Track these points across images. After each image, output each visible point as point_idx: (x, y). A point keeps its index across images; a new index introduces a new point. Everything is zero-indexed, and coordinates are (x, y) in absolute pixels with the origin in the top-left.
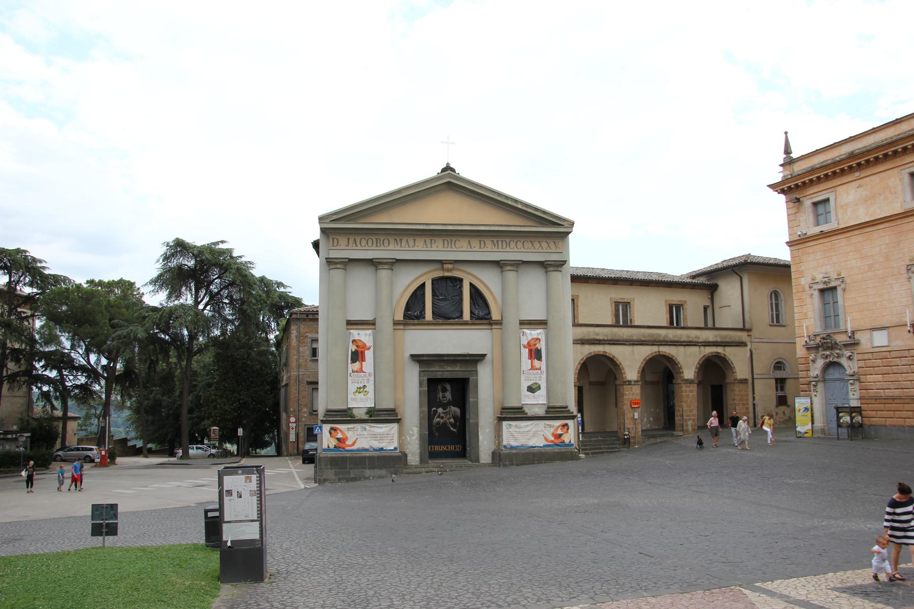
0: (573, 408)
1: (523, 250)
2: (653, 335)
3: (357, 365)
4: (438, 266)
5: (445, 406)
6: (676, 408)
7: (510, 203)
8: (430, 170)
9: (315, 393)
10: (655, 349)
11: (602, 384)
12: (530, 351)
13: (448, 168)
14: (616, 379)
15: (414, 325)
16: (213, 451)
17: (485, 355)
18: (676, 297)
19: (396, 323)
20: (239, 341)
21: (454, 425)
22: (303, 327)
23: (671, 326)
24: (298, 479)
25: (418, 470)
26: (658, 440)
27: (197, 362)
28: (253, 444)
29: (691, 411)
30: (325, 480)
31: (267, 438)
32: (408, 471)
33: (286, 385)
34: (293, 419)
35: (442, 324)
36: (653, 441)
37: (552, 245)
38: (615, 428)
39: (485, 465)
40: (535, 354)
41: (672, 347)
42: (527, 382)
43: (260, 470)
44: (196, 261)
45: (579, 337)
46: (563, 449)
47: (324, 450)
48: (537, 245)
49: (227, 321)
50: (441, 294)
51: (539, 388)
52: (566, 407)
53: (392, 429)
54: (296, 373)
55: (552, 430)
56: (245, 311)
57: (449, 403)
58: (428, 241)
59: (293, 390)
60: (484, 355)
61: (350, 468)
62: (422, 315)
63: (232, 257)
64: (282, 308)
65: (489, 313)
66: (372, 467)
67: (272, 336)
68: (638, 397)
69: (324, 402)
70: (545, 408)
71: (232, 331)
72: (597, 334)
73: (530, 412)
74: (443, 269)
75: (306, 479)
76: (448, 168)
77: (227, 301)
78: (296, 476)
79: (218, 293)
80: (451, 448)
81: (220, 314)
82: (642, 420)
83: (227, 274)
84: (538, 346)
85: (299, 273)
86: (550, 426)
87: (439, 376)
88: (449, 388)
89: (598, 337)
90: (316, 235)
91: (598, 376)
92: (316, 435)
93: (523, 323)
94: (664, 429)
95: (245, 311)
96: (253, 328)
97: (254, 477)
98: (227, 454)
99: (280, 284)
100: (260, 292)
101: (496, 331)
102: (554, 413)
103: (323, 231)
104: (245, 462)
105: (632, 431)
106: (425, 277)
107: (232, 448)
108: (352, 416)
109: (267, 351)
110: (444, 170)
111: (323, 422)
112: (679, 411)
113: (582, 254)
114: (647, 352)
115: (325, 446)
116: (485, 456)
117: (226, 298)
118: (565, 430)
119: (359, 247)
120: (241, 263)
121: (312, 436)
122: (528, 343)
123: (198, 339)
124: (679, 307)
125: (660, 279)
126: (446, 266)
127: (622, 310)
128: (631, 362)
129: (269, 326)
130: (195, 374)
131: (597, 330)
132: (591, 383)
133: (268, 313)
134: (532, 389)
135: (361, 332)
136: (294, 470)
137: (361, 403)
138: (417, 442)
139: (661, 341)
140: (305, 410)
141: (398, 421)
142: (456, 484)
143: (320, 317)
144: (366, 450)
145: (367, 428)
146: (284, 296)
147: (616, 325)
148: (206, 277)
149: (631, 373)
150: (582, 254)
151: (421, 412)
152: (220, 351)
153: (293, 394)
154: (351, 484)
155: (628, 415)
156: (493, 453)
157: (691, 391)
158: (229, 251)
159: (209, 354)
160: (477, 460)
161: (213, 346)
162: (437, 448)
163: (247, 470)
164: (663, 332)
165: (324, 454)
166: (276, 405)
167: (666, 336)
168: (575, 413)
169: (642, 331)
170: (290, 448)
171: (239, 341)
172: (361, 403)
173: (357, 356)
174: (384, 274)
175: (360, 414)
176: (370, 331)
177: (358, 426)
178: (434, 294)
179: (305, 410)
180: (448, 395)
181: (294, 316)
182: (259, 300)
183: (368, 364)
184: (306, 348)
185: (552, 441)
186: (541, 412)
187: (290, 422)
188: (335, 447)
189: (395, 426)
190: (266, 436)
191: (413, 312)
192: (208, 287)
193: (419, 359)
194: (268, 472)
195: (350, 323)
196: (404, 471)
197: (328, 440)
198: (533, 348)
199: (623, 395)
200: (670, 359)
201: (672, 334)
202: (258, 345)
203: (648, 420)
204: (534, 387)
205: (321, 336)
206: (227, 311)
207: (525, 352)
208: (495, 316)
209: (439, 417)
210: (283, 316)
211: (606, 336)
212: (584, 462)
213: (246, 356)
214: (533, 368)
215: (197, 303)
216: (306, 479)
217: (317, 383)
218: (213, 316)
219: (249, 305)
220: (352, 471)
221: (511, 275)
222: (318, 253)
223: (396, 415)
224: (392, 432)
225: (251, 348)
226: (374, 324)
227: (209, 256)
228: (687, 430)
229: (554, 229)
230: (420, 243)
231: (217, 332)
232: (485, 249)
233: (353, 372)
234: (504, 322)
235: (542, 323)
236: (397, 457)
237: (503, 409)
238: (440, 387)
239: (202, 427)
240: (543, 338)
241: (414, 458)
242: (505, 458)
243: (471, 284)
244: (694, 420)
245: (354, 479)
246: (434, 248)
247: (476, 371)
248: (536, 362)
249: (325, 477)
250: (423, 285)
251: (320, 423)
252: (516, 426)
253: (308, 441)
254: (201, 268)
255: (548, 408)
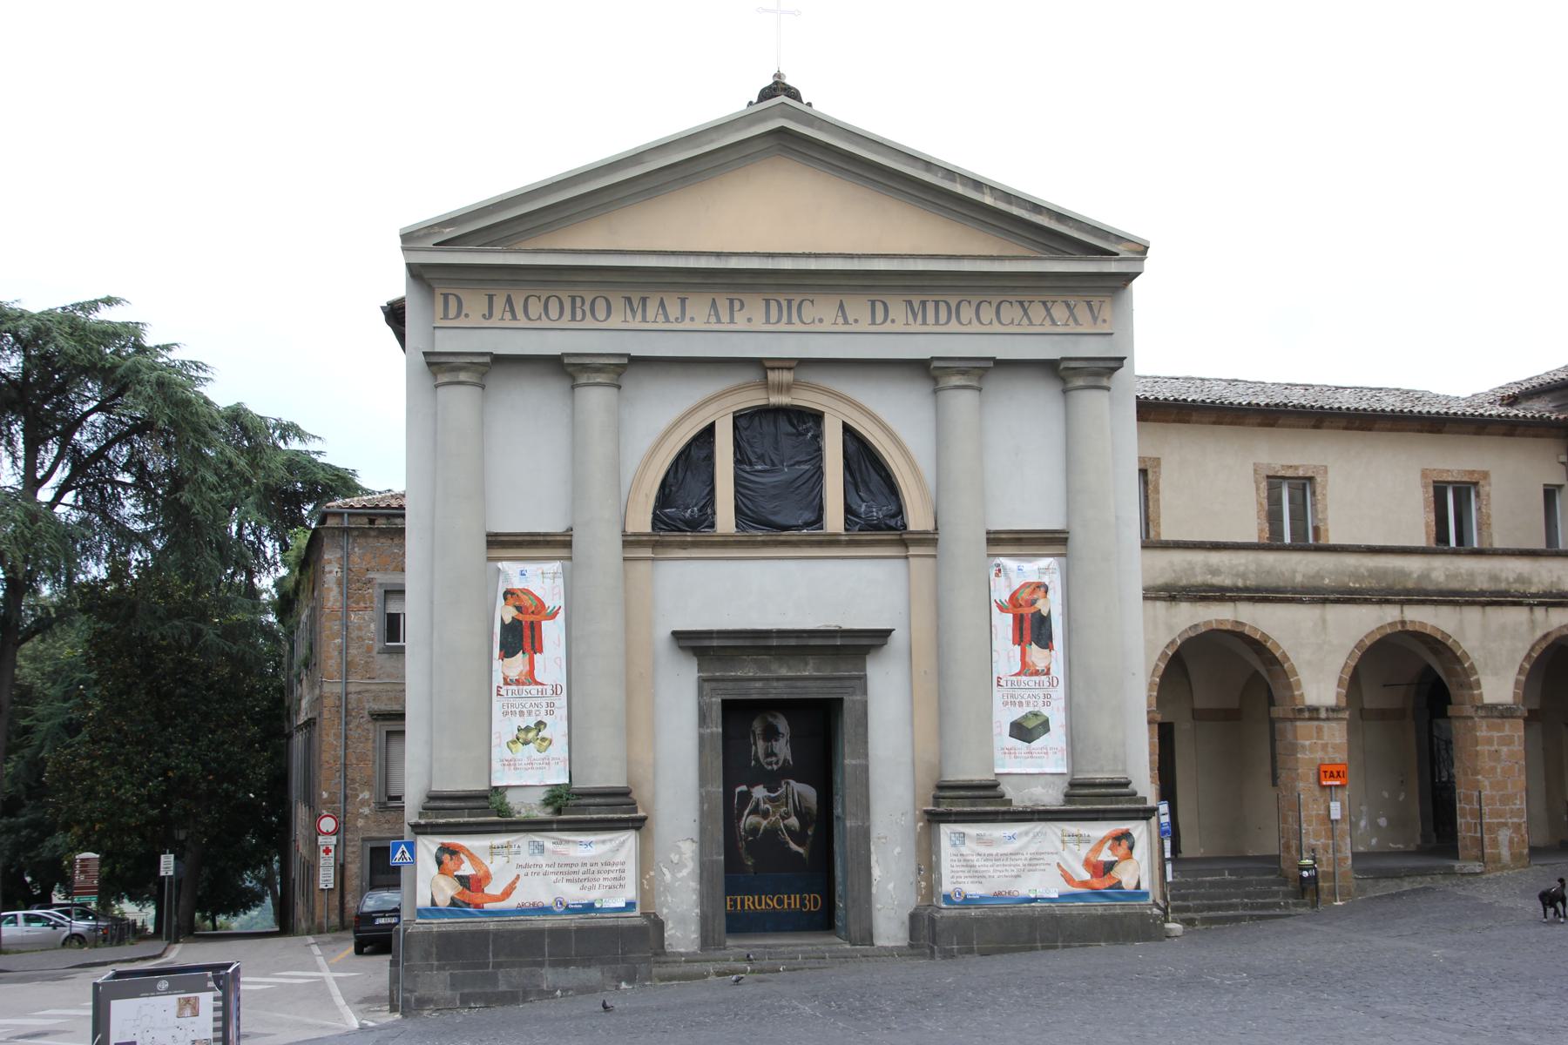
0: (1145, 786)
1: (997, 328)
2: (1385, 572)
3: (517, 664)
4: (752, 375)
5: (772, 780)
6: (1461, 791)
7: (959, 189)
8: (723, 96)
9: (394, 747)
10: (1391, 614)
11: (1230, 716)
12: (1019, 621)
13: (777, 88)
14: (1271, 702)
15: (683, 545)
16: (81, 926)
17: (888, 632)
18: (1455, 460)
19: (631, 542)
20: (165, 596)
21: (798, 837)
22: (359, 554)
23: (1440, 544)
24: (340, 1001)
25: (696, 967)
26: (1406, 885)
27: (34, 659)
28: (203, 903)
29: (1505, 800)
30: (422, 1003)
31: (249, 882)
32: (665, 970)
33: (310, 723)
34: (328, 824)
35: (765, 544)
36: (1390, 886)
37: (1082, 312)
38: (1271, 847)
39: (889, 952)
40: (1033, 629)
41: (1445, 611)
42: (1011, 708)
43: (224, 979)
44: (27, 358)
45: (1160, 581)
46: (1118, 908)
47: (421, 913)
48: (1037, 312)
49: (130, 538)
50: (761, 458)
51: (1045, 726)
52: (1126, 784)
53: (613, 850)
54: (338, 689)
55: (1084, 851)
56: (187, 508)
57: (786, 772)
58: (722, 304)
59: (330, 740)
60: (886, 633)
61: (498, 966)
62: (704, 519)
63: (141, 349)
64: (296, 500)
65: (900, 511)
66: (562, 962)
67: (265, 582)
68: (1341, 757)
69: (420, 771)
70: (1061, 787)
71: (143, 567)
72: (1215, 572)
73: (1019, 797)
74: (766, 385)
75: (366, 1000)
76: (777, 88)
77: (127, 478)
78: (335, 991)
79: (100, 454)
80: (792, 902)
81: (105, 516)
82: (1354, 825)
83: (128, 398)
84: (1041, 605)
85: (355, 410)
86: (1080, 840)
87: (755, 692)
88: (784, 728)
89: (1217, 581)
90: (397, 286)
91: (1218, 693)
92: (397, 869)
93: (998, 540)
94: (1421, 852)
95: (187, 508)
96: (210, 557)
97: (207, 1001)
98: (125, 932)
99: (289, 430)
100: (230, 453)
101: (920, 565)
102: (1090, 799)
103: (416, 273)
104: (179, 954)
105: (1325, 858)
106: (712, 408)
107: (140, 913)
108: (503, 810)
109: (253, 623)
110: (766, 94)
111: (419, 829)
112: (1469, 799)
113: (1174, 334)
114: (1366, 621)
115: (423, 901)
116: (889, 928)
117: (126, 469)
118: (1123, 850)
119: (523, 322)
120: (169, 366)
121: (384, 871)
122: (1013, 596)
123: (37, 592)
124: (1464, 490)
125: (1407, 406)
126: (773, 376)
127: (1291, 508)
128: (1318, 653)
129: (258, 552)
130: (27, 695)
131: (1215, 558)
132: (1198, 715)
133: (255, 516)
134: (1024, 731)
135: (531, 568)
136: (328, 975)
137: (528, 773)
138: (694, 884)
139: (1408, 592)
140: (366, 795)
141: (638, 824)
142: (807, 1009)
143: (410, 523)
144: (545, 910)
145: (548, 844)
146: (300, 465)
147: (1273, 544)
148: (59, 406)
149: (1319, 682)
150: (1174, 334)
151: (703, 799)
152: (107, 626)
153: (329, 751)
154: (498, 1011)
155: (1311, 810)
156: (914, 917)
157: (1507, 741)
158: (131, 332)
159: (72, 636)
160: (868, 937)
161: (84, 611)
162: (750, 902)
163: (184, 978)
164: (1414, 565)
165: (419, 926)
166: (279, 781)
167: (1425, 576)
168: (1152, 801)
169: (1351, 561)
170: (320, 911)
171: (165, 596)
172: (528, 773)
173: (519, 637)
174: (595, 398)
175: (528, 805)
176: (556, 566)
177: (521, 841)
178: (740, 458)
179: (366, 795)
180: (783, 749)
181: (331, 522)
182: (220, 476)
183: (551, 662)
184: (367, 615)
185: (1084, 884)
186: (1052, 797)
187: (319, 832)
188: (454, 903)
189: (629, 839)
190: (248, 875)
191: (679, 513)
192: (65, 437)
193: (691, 643)
194: (249, 984)
195: (499, 543)
196: (655, 970)
197: (433, 882)
198: (1027, 611)
199: (1293, 749)
200: (1436, 645)
201: (1441, 570)
202: (225, 606)
203: (1373, 824)
204: (1031, 724)
205: (413, 582)
206: (129, 508)
207: (1004, 624)
208: (917, 519)
209: (755, 811)
210: (298, 521)
211: (1243, 575)
212: (1180, 946)
213: (187, 639)
214: (1026, 669)
215: (32, 483)
216: (366, 1000)
217: (401, 716)
218: (84, 522)
219: (197, 491)
220: (501, 973)
221: (961, 402)
222: (401, 337)
223: (632, 806)
224: (620, 858)
225: (203, 616)
226: (568, 544)
227: (69, 345)
228: (1497, 859)
229: (1083, 265)
230: (699, 310)
231: (96, 571)
232: (888, 327)
233: (507, 682)
234: (943, 536)
235: (1052, 541)
236: (634, 928)
237: (940, 787)
238: (757, 726)
239: (46, 854)
240: (1055, 582)
241: (682, 935)
242: (944, 931)
243: (847, 429)
244: (1517, 827)
245: (510, 998)
246: (741, 323)
247: (863, 678)
248: (1037, 655)
249: (421, 992)
250: (709, 431)
251: (408, 834)
252: (980, 839)
253: (374, 886)
254: (45, 379)
255: (1072, 785)
